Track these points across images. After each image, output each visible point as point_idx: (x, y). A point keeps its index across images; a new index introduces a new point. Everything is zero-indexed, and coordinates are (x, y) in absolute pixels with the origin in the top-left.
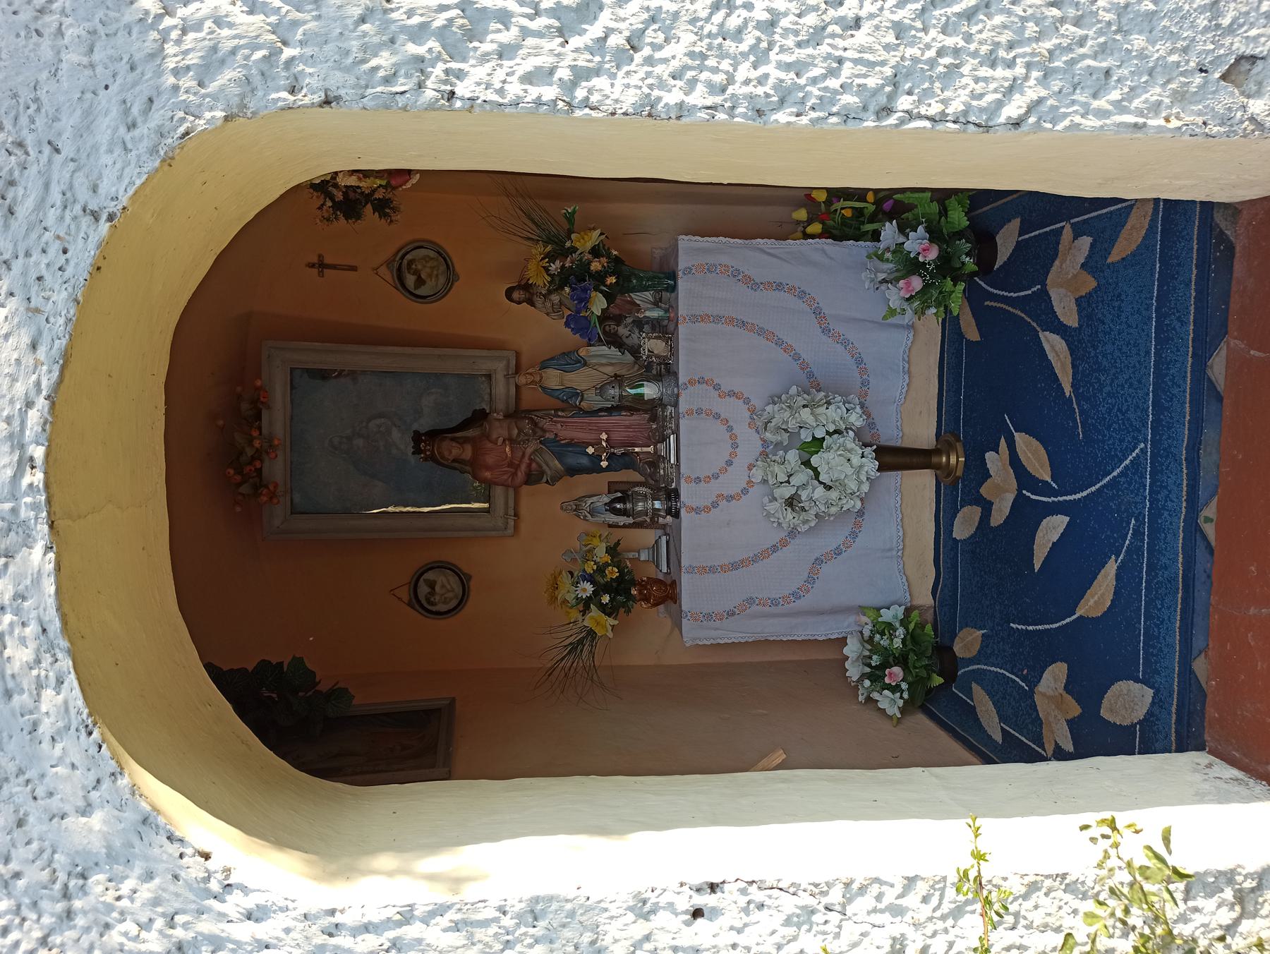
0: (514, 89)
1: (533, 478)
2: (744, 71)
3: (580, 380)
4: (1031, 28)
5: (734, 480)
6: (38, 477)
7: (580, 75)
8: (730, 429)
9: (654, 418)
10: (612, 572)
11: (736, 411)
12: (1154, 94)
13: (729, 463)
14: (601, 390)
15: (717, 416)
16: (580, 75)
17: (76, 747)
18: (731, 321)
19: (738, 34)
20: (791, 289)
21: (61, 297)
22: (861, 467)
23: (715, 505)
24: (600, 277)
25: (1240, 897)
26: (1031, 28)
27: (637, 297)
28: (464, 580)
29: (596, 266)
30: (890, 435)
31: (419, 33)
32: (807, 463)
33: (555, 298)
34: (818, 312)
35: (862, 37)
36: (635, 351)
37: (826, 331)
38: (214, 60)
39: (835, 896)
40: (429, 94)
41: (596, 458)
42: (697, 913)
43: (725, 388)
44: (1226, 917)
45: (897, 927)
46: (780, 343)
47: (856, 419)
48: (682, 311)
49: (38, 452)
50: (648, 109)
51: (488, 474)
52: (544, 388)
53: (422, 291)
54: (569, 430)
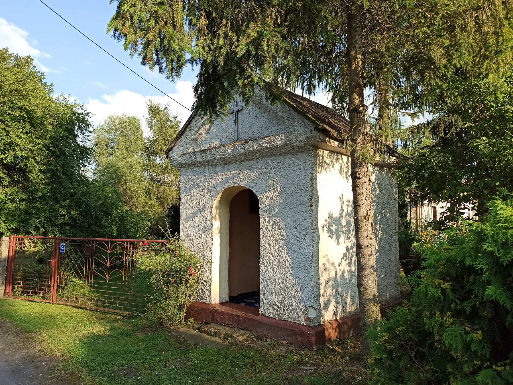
38: (262, 198)
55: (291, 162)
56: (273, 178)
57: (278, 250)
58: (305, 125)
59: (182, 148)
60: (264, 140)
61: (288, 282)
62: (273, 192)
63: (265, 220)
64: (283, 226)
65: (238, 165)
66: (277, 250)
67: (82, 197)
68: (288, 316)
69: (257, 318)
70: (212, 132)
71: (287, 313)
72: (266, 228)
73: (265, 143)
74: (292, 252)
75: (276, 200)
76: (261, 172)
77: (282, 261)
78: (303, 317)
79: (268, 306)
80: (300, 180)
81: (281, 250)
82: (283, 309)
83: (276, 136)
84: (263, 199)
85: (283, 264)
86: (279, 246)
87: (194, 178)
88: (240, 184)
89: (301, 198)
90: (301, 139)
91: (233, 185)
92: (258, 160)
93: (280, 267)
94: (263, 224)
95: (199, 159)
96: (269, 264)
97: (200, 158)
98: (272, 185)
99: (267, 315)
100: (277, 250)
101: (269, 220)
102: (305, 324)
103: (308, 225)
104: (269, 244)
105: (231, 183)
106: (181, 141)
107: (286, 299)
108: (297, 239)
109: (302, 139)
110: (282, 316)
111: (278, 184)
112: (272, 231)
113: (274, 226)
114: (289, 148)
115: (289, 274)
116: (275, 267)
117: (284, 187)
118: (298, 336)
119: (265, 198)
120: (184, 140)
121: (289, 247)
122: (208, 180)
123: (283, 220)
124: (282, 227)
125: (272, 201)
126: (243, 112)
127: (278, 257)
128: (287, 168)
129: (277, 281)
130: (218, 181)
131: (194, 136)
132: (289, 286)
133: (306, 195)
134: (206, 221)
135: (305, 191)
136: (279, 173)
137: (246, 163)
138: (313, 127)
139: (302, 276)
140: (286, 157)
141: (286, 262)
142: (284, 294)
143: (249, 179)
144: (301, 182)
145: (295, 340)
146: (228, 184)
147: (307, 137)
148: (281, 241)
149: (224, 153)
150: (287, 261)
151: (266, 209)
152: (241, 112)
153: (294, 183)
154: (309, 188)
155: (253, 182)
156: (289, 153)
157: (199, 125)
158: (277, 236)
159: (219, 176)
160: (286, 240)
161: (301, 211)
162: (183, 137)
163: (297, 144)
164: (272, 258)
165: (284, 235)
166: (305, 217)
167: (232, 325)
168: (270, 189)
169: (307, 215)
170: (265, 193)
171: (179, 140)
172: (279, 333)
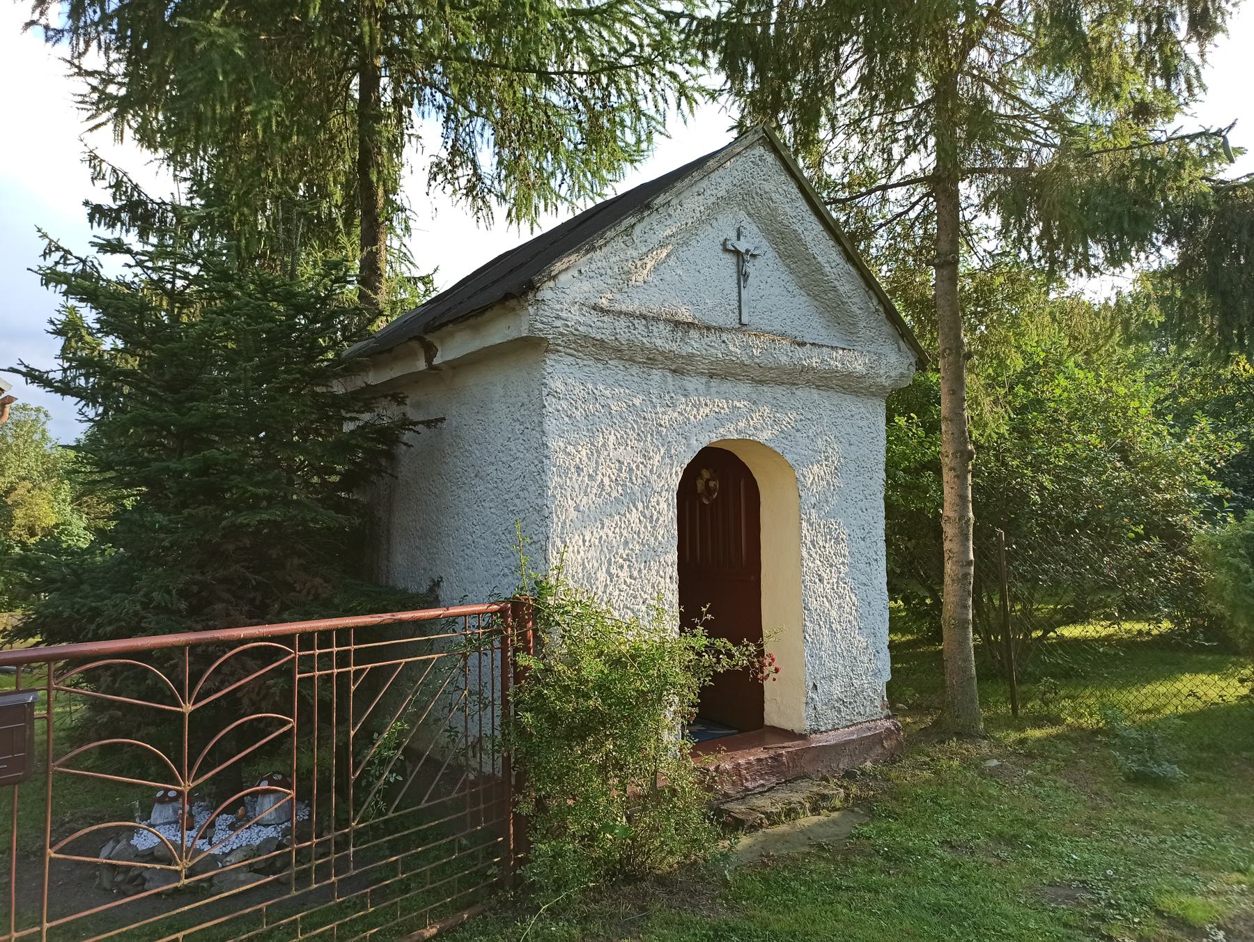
38: (804, 477)
59: (586, 286)
65: (745, 388)
67: (277, 400)
87: (607, 393)
89: (871, 482)
91: (736, 437)
92: (794, 388)
95: (659, 342)
97: (661, 339)
98: (824, 449)
101: (819, 525)
104: (820, 575)
105: (732, 429)
109: (893, 374)
120: (599, 264)
122: (659, 409)
130: (692, 418)
134: (654, 528)
137: (765, 389)
146: (721, 430)
149: (739, 352)
151: (813, 500)
153: (861, 451)
157: (654, 239)
160: (850, 565)
164: (827, 604)
167: (763, 785)
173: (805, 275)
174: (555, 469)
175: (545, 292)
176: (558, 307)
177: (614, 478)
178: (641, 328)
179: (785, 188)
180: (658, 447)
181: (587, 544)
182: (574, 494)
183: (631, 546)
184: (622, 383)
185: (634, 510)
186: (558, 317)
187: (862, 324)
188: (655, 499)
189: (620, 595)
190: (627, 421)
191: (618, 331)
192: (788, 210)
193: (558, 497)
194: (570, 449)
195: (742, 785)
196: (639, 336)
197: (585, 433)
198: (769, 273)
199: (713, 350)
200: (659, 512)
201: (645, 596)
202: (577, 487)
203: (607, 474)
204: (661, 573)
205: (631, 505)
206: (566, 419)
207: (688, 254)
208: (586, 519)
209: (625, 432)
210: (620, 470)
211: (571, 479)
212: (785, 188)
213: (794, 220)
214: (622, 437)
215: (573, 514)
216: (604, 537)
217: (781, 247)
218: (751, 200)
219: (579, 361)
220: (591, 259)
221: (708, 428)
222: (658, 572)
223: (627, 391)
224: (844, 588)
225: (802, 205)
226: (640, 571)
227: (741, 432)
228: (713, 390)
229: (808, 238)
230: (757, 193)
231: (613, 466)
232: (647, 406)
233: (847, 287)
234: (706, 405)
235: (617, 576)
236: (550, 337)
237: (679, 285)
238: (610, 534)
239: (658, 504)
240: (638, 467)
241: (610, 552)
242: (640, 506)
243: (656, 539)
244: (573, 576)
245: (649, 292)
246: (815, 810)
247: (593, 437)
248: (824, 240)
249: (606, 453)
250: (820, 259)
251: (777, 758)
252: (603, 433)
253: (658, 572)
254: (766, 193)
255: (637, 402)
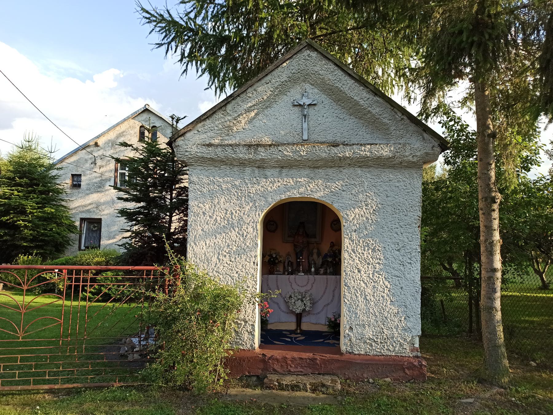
0: (346, 244)
1: (295, 246)
2: (349, 269)
3: (315, 256)
4: (355, 302)
5: (295, 286)
6: (306, 196)
7: (348, 251)
8: (305, 286)
9: (307, 271)
10: (277, 261)
11: (309, 287)
12: (348, 318)
13: (298, 285)
14: (313, 260)
15: (308, 283)
16: (348, 251)
17: (278, 198)
18: (327, 286)
19: (353, 269)
20: (333, 299)
21: (324, 199)
22: (298, 309)
23: (290, 282)
24: (335, 260)
25: (251, 332)
26: (355, 302)
27: (331, 268)
28: (274, 231)
29: (337, 259)
30: (304, 319)
31: (351, 235)
32: (299, 299)
33: (331, 252)
34: (328, 304)
35: (353, 282)
36: (321, 268)
37: (325, 306)
38: (347, 215)
39: (255, 279)
40: (345, 236)
41: (300, 259)
42: (254, 263)
43: (313, 285)
44: (249, 330)
45: (251, 287)
46: (322, 296)
47: (307, 309)
48: (329, 276)
49: (309, 196)
50: (345, 259)
51: (296, 237)
52: (313, 249)
53: (333, 225)
54: (305, 254)
55: (392, 176)
56: (366, 192)
57: (373, 276)
58: (424, 139)
59: (203, 136)
60: (363, 148)
61: (388, 312)
62: (366, 209)
63: (353, 241)
64: (380, 249)
65: (307, 172)
66: (371, 276)
68: (388, 350)
69: (343, 358)
70: (257, 123)
71: (386, 346)
72: (353, 250)
73: (365, 151)
74: (393, 277)
75: (370, 218)
76: (347, 183)
77: (379, 288)
78: (408, 349)
79: (358, 341)
80: (406, 198)
81: (378, 276)
82: (381, 343)
83: (382, 146)
84: (349, 216)
85: (380, 291)
86: (374, 271)
87: (221, 180)
88: (310, 194)
89: (406, 218)
90: (417, 154)
91: (298, 196)
92: (341, 169)
93: (375, 295)
94: (348, 245)
95: (241, 156)
96: (359, 293)
99: (357, 353)
100: (371, 276)
101: (359, 241)
102: (411, 356)
103: (415, 247)
105: (295, 192)
106: (204, 126)
107: (385, 330)
108: (400, 263)
110: (379, 350)
111: (373, 200)
112: (363, 254)
113: (366, 248)
114: (398, 161)
115: (389, 303)
116: (368, 295)
117: (382, 204)
118: (406, 370)
119: (353, 215)
121: (390, 272)
123: (380, 242)
124: (378, 250)
125: (364, 219)
126: (316, 108)
127: (373, 284)
128: (387, 183)
129: (371, 310)
131: (228, 123)
132: (389, 315)
133: (413, 215)
134: (244, 239)
135: (412, 211)
136: (374, 188)
137: (320, 171)
138: (436, 144)
139: (408, 303)
140: (385, 170)
141: (385, 289)
142: (382, 326)
143: (327, 190)
144: (406, 200)
145: (402, 374)
146: (288, 193)
147: (426, 153)
148: (377, 265)
149: (291, 154)
150: (387, 287)
151: (354, 228)
152: (313, 107)
154: (417, 208)
155: (332, 194)
156: (407, 167)
158: (371, 259)
159: (273, 183)
160: (384, 265)
161: (406, 232)
162: (208, 122)
163: (410, 158)
164: (363, 285)
165: (382, 258)
166: (410, 239)
167: (301, 372)
168: (361, 205)
169: (414, 236)
170: (353, 209)
171: (200, 125)
172: (380, 371)
173: (351, 108)
174: (192, 214)
175: (179, 142)
176: (186, 147)
177: (223, 217)
178: (229, 151)
179: (326, 67)
180: (248, 203)
181: (207, 245)
182: (201, 224)
183: (231, 247)
184: (229, 175)
185: (233, 231)
186: (186, 151)
187: (392, 128)
188: (246, 226)
189: (223, 268)
190: (231, 192)
191: (218, 153)
192: (330, 77)
193: (193, 225)
194: (201, 205)
195: (287, 368)
196: (230, 154)
197: (209, 198)
198: (325, 112)
199: (275, 156)
200: (247, 232)
201: (238, 270)
202: (203, 221)
203: (219, 216)
204: (248, 260)
205: (232, 229)
206: (199, 193)
207: (271, 112)
208: (207, 235)
209: (230, 197)
210: (226, 213)
211: (200, 218)
212: (326, 67)
213: (335, 81)
214: (228, 199)
215: (200, 232)
216: (217, 243)
217: (333, 97)
218: (310, 77)
219: (205, 168)
220: (204, 124)
221: (279, 193)
222: (246, 260)
223: (231, 179)
224: (379, 277)
225: (339, 73)
226: (235, 258)
227: (301, 194)
228: (284, 174)
229: (345, 89)
230: (312, 73)
231: (222, 212)
232: (243, 184)
233: (378, 110)
234: (278, 181)
235: (222, 260)
236: (185, 160)
237: (264, 127)
238: (220, 241)
239: (247, 229)
240: (236, 212)
241: (219, 249)
242: (237, 229)
243: (245, 244)
244: (200, 258)
245: (245, 133)
246: (314, 390)
247: (213, 200)
248: (356, 88)
249: (219, 206)
250: (355, 98)
251: (313, 360)
252: (218, 197)
253: (246, 260)
254: (316, 72)
255: (237, 183)
